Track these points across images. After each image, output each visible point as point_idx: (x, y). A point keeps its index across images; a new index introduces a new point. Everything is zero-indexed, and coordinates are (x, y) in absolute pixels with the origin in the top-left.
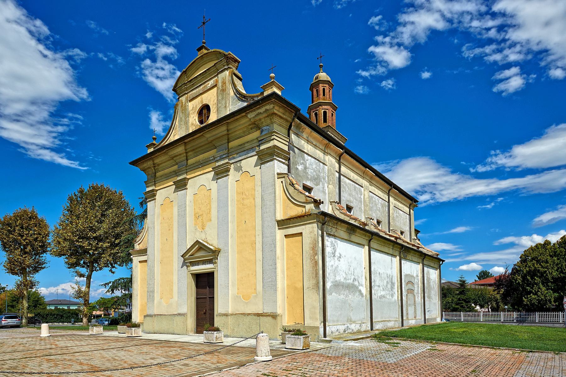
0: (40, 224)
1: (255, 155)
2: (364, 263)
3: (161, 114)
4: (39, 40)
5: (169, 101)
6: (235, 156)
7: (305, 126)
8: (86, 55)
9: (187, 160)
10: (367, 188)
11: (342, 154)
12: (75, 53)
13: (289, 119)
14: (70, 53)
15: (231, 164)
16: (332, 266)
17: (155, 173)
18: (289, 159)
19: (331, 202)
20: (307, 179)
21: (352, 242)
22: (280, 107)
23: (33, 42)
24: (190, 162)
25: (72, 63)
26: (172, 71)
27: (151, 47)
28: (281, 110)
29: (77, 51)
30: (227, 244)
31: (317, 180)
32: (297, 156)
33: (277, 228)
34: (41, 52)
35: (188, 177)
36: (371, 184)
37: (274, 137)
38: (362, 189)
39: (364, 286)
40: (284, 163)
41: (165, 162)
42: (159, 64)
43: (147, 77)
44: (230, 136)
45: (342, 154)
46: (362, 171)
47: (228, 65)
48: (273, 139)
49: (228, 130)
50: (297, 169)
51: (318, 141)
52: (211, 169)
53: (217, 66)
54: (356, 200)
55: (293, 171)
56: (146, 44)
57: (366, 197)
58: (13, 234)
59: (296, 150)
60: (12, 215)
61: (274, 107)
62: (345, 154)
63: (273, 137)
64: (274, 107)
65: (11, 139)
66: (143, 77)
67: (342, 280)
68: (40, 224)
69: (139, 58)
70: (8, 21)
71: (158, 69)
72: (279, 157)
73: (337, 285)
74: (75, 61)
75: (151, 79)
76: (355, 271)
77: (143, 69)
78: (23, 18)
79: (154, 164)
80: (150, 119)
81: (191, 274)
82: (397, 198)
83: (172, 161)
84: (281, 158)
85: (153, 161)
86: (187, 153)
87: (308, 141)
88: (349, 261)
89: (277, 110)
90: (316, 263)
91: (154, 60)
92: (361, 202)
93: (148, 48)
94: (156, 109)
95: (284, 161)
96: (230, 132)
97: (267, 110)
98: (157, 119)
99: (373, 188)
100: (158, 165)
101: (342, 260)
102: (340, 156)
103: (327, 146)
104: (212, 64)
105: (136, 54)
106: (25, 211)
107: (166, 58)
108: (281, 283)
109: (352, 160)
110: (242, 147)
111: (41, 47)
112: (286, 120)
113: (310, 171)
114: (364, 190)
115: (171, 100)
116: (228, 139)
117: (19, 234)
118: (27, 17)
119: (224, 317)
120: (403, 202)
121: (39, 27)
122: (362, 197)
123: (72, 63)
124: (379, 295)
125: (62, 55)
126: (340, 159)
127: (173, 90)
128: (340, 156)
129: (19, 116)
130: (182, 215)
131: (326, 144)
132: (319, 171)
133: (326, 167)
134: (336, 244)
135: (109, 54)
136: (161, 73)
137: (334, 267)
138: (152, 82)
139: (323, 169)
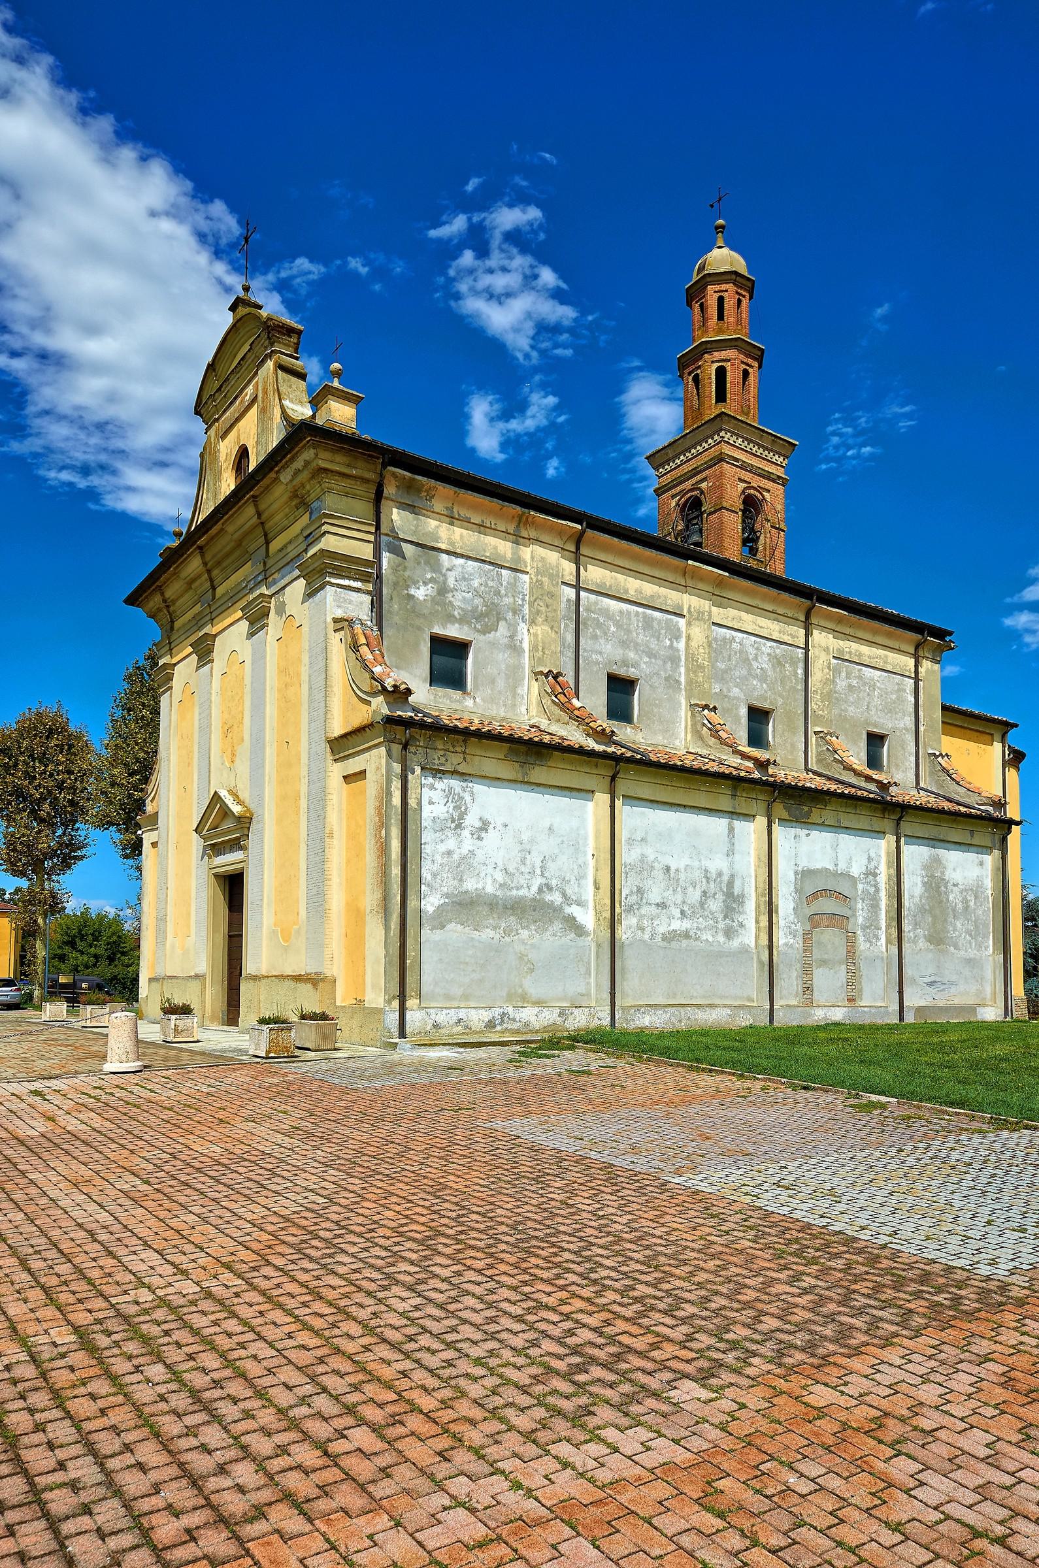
0: (72, 745)
1: (298, 577)
2: (591, 842)
3: (498, 401)
4: (218, 253)
5: (520, 356)
6: (276, 576)
7: (432, 482)
8: (323, 269)
9: (214, 588)
10: (697, 617)
11: (581, 534)
12: (295, 271)
13: (371, 476)
14: (283, 274)
15: (271, 597)
16: (449, 853)
17: (172, 622)
18: (379, 576)
19: (536, 674)
20: (450, 619)
21: (539, 785)
22: (332, 451)
23: (203, 258)
24: (220, 591)
25: (290, 295)
26: (528, 272)
27: (476, 218)
28: (339, 458)
29: (303, 263)
30: (261, 803)
31: (488, 616)
32: (409, 564)
33: (330, 757)
34: (220, 282)
35: (214, 631)
36: (720, 601)
37: (325, 528)
38: (682, 622)
39: (591, 904)
40: (357, 590)
41: (182, 596)
42: (494, 261)
43: (461, 302)
44: (267, 526)
45: (581, 534)
46: (675, 570)
47: (272, 345)
48: (325, 533)
49: (259, 515)
50: (411, 597)
51: (490, 512)
52: (239, 614)
53: (256, 349)
54: (651, 655)
55: (392, 607)
56: (464, 212)
57: (694, 644)
58: (12, 775)
59: (408, 549)
60: (15, 726)
61: (317, 455)
62: (590, 532)
63: (325, 528)
64: (317, 455)
65: (144, 514)
66: (452, 303)
67: (490, 889)
68: (70, 746)
69: (449, 251)
70: (153, 214)
71: (491, 271)
72: (343, 577)
73: (466, 906)
74: (295, 292)
75: (474, 305)
76: (551, 865)
77: (454, 280)
78: (183, 201)
79: (165, 601)
80: (467, 417)
81: (216, 875)
82: (847, 630)
83: (191, 592)
84: (350, 578)
85: (162, 594)
86: (209, 571)
87: (452, 519)
88: (525, 837)
89: (326, 459)
90: (384, 849)
91: (483, 252)
92: (675, 660)
93: (469, 219)
94: (482, 387)
95: (358, 584)
96: (264, 517)
97: (307, 463)
98: (487, 415)
99: (732, 612)
100: (174, 602)
101: (491, 837)
102: (579, 540)
103: (521, 521)
104: (247, 347)
105: (439, 241)
106: (39, 714)
107: (515, 238)
108: (337, 899)
109: (624, 544)
110: (284, 552)
111: (220, 268)
112: (366, 481)
113: (458, 600)
114: (689, 624)
115: (527, 356)
116: (266, 535)
117: (27, 772)
118: (194, 197)
119: (629, 961)
120: (860, 634)
121: (219, 220)
122: (681, 645)
123: (290, 295)
124: (662, 929)
125: (267, 282)
126: (578, 548)
127: (197, 413)
128: (579, 540)
129: (167, 450)
130: (205, 729)
131: (520, 517)
132: (497, 593)
133: (526, 578)
134: (467, 798)
135: (372, 256)
136: (500, 282)
137: (456, 857)
138: (477, 315)
139: (513, 585)
